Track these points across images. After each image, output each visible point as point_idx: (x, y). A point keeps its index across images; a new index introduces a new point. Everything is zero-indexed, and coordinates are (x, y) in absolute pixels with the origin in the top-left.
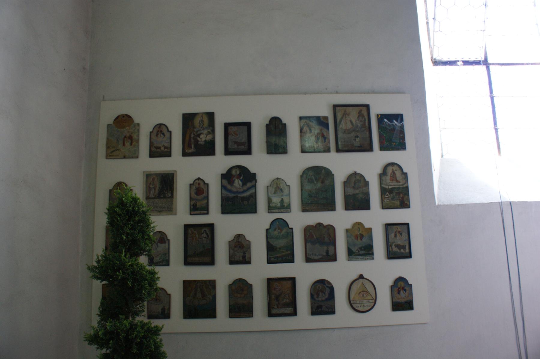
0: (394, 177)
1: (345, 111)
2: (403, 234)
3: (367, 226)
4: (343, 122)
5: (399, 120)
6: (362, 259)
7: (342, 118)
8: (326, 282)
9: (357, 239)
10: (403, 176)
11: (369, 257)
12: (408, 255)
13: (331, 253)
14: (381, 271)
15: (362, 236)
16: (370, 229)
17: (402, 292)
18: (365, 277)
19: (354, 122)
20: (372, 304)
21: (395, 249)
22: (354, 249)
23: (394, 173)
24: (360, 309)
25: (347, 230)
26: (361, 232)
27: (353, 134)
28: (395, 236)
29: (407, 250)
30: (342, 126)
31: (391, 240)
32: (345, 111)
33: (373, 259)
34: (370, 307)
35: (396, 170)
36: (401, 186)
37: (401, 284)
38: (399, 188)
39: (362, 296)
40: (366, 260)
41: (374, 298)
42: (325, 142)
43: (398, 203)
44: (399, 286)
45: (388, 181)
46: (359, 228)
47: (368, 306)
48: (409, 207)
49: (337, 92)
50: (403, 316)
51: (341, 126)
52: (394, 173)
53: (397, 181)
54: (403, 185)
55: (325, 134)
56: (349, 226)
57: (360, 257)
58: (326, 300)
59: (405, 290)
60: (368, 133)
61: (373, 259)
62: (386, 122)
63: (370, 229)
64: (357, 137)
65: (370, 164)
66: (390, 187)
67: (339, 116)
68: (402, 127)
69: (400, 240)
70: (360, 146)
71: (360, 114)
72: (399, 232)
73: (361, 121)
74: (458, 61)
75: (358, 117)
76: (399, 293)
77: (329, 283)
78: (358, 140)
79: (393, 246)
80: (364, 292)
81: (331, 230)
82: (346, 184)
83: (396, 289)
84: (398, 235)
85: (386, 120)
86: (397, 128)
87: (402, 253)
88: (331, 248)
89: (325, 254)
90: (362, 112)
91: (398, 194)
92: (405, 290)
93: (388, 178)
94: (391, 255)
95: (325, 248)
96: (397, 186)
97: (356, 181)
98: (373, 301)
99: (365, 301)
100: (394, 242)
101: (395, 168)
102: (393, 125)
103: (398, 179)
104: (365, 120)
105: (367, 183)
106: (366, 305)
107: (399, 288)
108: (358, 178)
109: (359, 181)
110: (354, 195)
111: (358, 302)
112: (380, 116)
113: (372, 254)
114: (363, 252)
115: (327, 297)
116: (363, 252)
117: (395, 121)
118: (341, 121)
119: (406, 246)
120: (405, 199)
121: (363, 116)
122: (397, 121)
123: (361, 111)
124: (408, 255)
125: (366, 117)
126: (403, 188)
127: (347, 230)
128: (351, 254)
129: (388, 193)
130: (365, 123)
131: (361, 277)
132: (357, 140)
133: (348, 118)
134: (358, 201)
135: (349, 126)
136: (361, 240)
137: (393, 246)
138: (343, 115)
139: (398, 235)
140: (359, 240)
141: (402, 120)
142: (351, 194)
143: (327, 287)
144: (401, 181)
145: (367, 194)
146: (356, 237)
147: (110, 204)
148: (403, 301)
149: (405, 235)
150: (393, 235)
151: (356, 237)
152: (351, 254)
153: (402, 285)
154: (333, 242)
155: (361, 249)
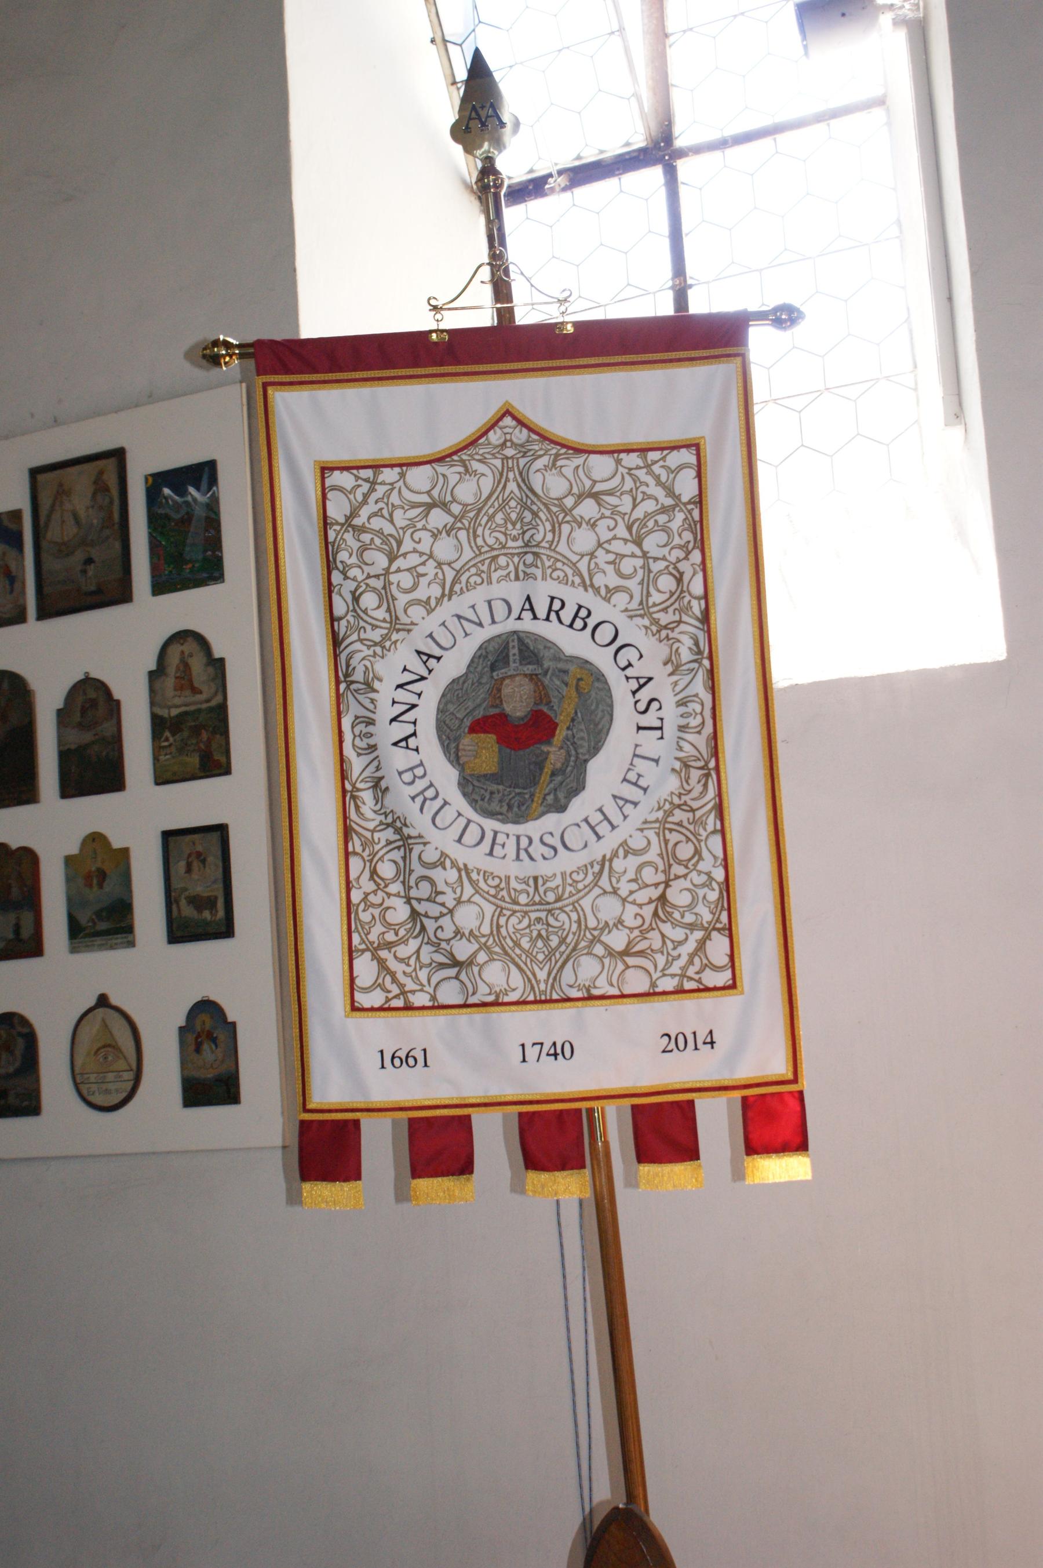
0: (186, 682)
1: (61, 485)
2: (210, 859)
3: (117, 844)
4: (56, 516)
5: (204, 485)
6: (102, 947)
7: (53, 506)
8: (16, 1021)
9: (91, 886)
10: (211, 670)
11: (119, 938)
12: (223, 929)
13: (26, 932)
14: (156, 979)
15: (102, 875)
16: (125, 852)
17: (206, 1047)
18: (114, 1001)
19: (82, 514)
20: (129, 1086)
21: (188, 911)
22: (83, 919)
23: (185, 666)
24: (98, 1099)
25: (69, 860)
26: (99, 864)
27: (79, 556)
28: (189, 869)
29: (221, 913)
30: (54, 533)
31: (176, 884)
32: (61, 485)
33: (132, 944)
34: (124, 1095)
35: (191, 655)
36: (204, 706)
37: (205, 1020)
38: (199, 711)
39: (109, 1064)
40: (112, 948)
41: (134, 1066)
42: (12, 591)
43: (194, 760)
44: (198, 1028)
45: (170, 692)
46: (95, 852)
47: (117, 1091)
48: (227, 771)
49: (56, 422)
50: (213, 1117)
51: (49, 535)
52: (185, 666)
53: (195, 691)
54: (208, 701)
55: (13, 567)
56: (74, 849)
57: (99, 941)
58: (18, 1072)
59: (215, 1041)
60: (117, 545)
61: (132, 944)
62: (166, 498)
63: (125, 852)
64: (89, 561)
65: (116, 646)
66: (174, 712)
67: (45, 502)
68: (213, 507)
69: (202, 884)
70: (99, 591)
71: (100, 487)
72: (199, 854)
73: (101, 508)
74: (550, 175)
75: (94, 494)
76: (198, 1049)
77: (24, 1021)
78: (91, 570)
79: (183, 902)
80: (108, 1047)
81: (28, 858)
82: (63, 716)
83: (190, 1038)
84: (196, 864)
85: (167, 491)
86: (199, 512)
87: (207, 923)
88: (27, 917)
89: (11, 936)
90: (105, 477)
91: (196, 731)
92: (215, 1041)
93: (169, 682)
94: (179, 932)
95: (12, 917)
96: (192, 708)
97: (91, 703)
98: (130, 1076)
99: (110, 1076)
100: (185, 889)
101: (190, 646)
102: (187, 503)
103: (196, 684)
104: (111, 502)
105: (114, 707)
106: (111, 1087)
107: (199, 1036)
108: (92, 694)
109: (93, 703)
110: (82, 749)
111: (93, 1078)
112: (150, 480)
113: (130, 929)
114: (103, 926)
115: (17, 1064)
116: (103, 926)
117: (192, 490)
118: (47, 525)
119: (216, 898)
120: (214, 746)
121: (107, 489)
122: (198, 489)
123: (101, 473)
124: (223, 929)
125: (115, 493)
126: (211, 710)
127: (69, 860)
128: (80, 933)
129: (167, 734)
130: (111, 512)
131: (103, 1001)
132: (90, 573)
133: (68, 506)
134: (94, 770)
135: (71, 530)
136: (101, 886)
137: (183, 902)
138: (56, 498)
139: (196, 864)
140: (95, 888)
141: (213, 480)
142: (73, 747)
143: (20, 1034)
144: (204, 688)
145: (116, 741)
146: (88, 877)
147: (570, 801)
148: (210, 1075)
149: (214, 859)
150: (182, 864)
151: (88, 877)
152: (80, 933)
153: (208, 1026)
154: (32, 900)
155: (98, 914)
